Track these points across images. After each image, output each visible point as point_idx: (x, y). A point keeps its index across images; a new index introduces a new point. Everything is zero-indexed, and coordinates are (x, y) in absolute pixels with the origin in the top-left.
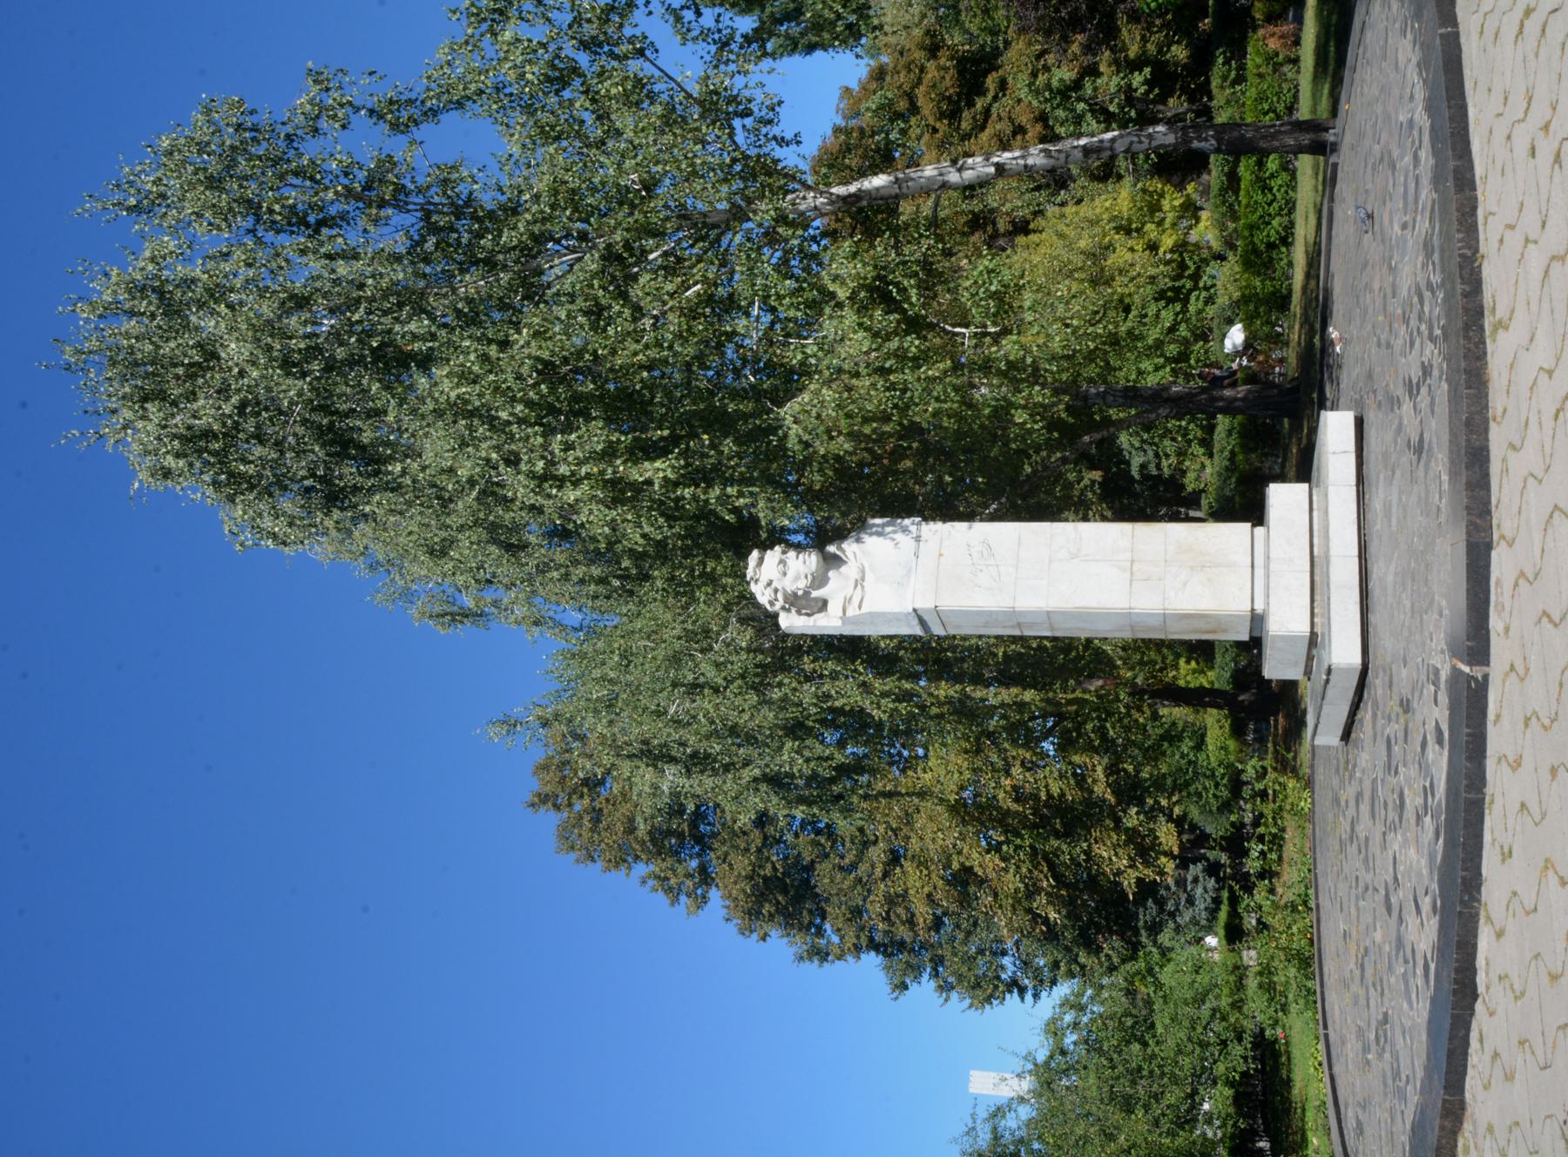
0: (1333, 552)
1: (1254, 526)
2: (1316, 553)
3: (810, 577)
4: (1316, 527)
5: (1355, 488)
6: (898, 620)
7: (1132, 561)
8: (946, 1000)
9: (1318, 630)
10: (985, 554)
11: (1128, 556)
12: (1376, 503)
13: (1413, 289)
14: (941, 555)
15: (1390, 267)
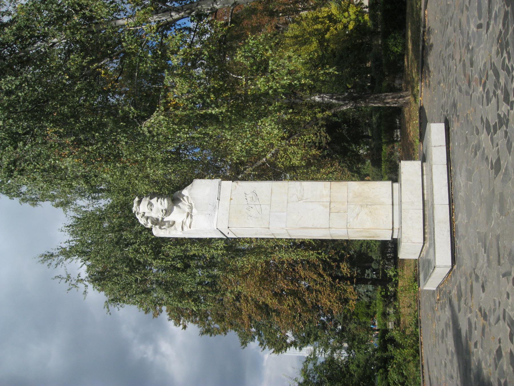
0: (435, 202)
2: (425, 199)
3: (164, 211)
4: (425, 184)
5: (446, 166)
6: (210, 232)
7: (330, 202)
8: (263, 349)
11: (328, 199)
12: (460, 180)
13: (488, 66)
14: (231, 199)
15: (469, 50)
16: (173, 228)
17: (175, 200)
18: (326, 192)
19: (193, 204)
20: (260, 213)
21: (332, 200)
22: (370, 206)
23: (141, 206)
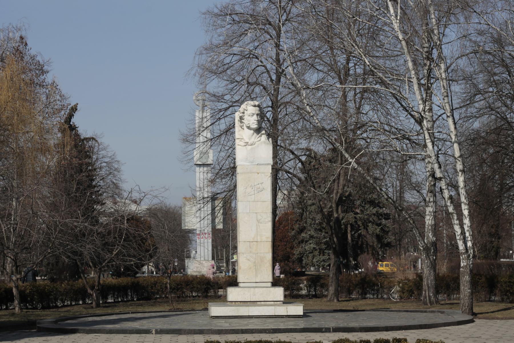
1: (272, 283)
5: (274, 315)
7: (257, 242)
9: (478, 315)
10: (259, 189)
11: (259, 240)
17: (258, 131)
18: (264, 239)
19: (254, 146)
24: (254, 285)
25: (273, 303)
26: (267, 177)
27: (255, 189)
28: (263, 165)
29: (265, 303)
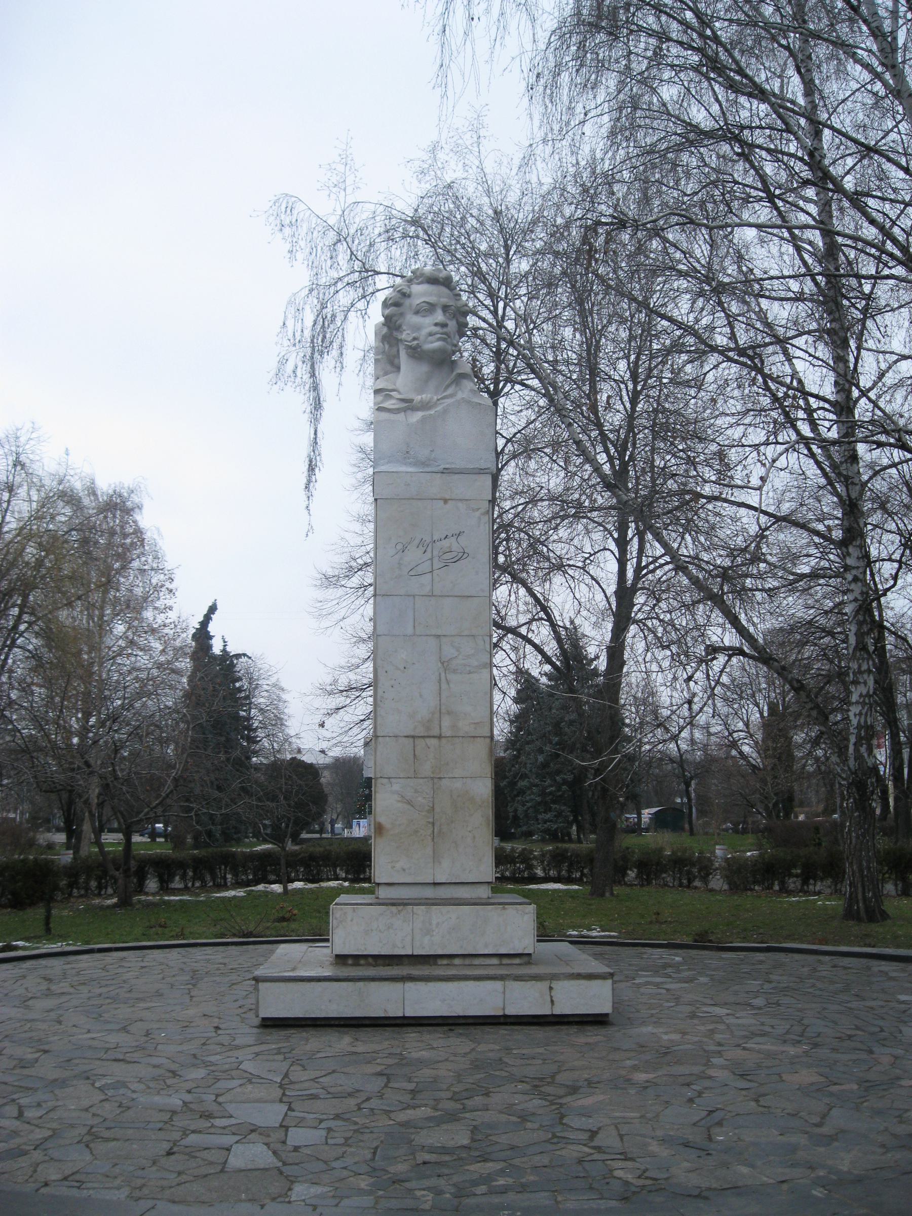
3: (415, 342)
16: (389, 368)
20: (412, 573)
21: (444, 741)
22: (430, 831)
23: (425, 287)
24: (429, 893)
25: (495, 961)
26: (478, 514)
27: (435, 553)
28: (460, 473)
29: (467, 961)
